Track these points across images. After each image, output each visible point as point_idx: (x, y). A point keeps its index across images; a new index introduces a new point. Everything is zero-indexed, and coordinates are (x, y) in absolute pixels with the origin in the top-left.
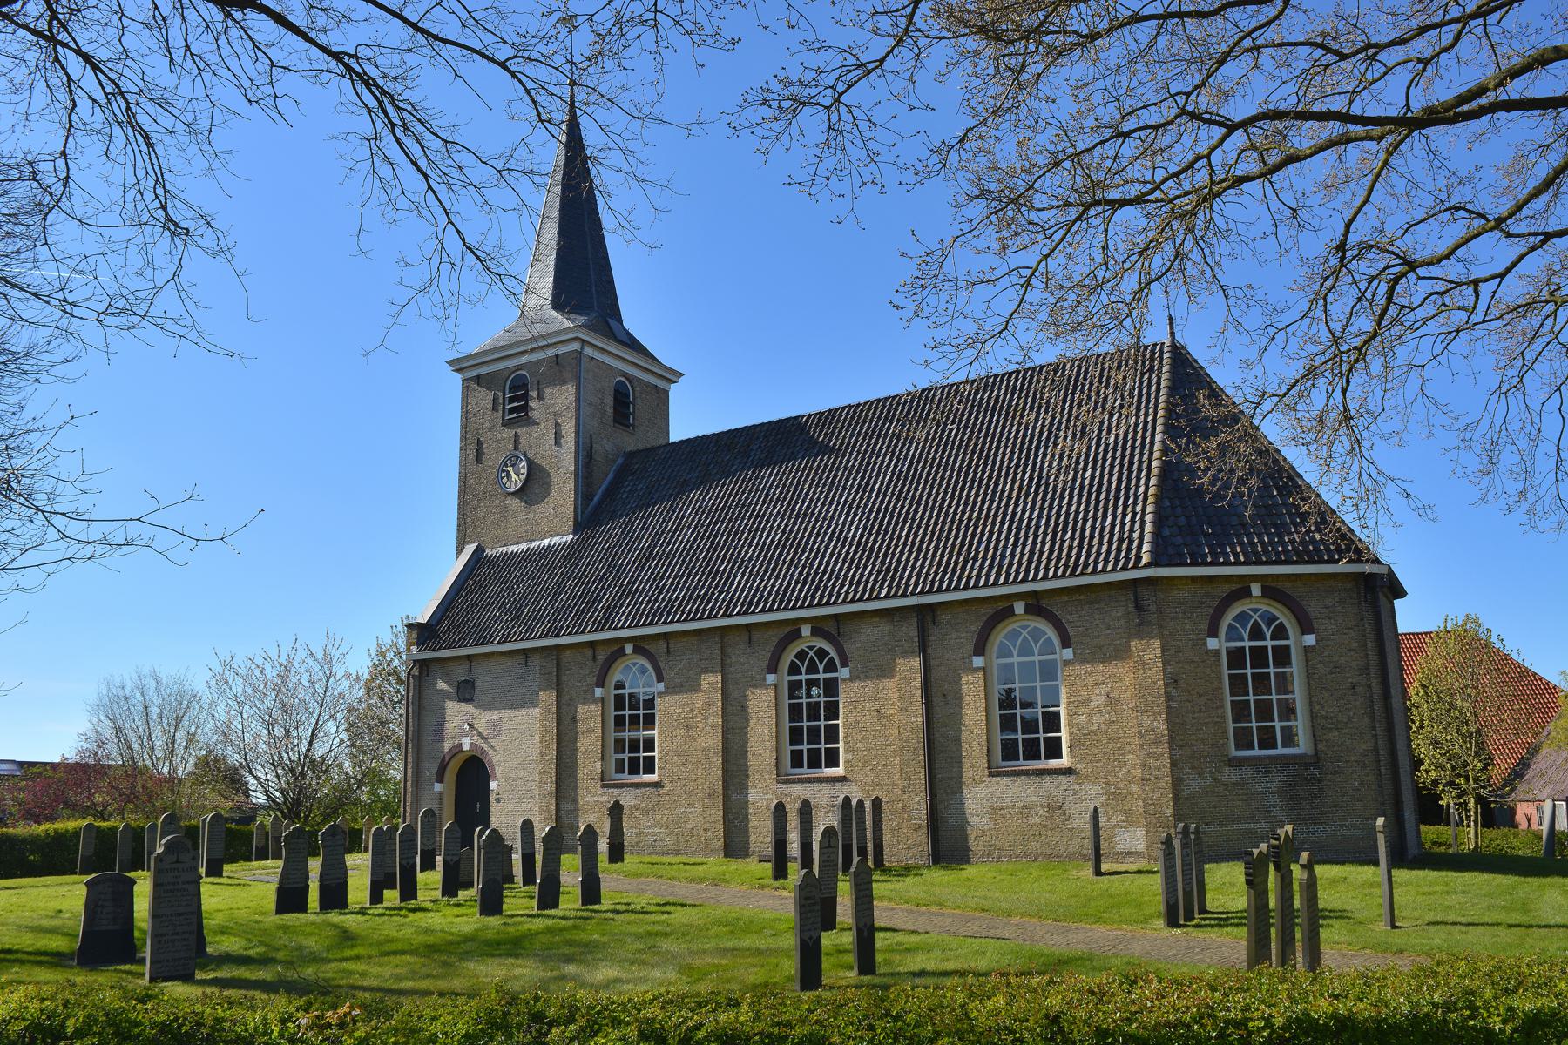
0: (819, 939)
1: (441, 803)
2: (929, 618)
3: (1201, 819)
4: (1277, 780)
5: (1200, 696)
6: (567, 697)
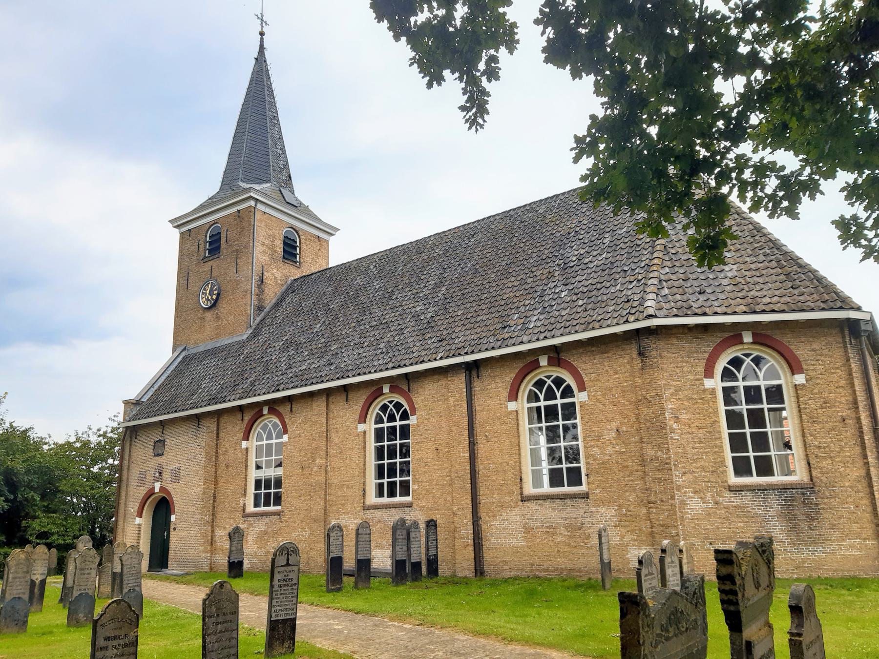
2: (474, 373)
3: (706, 538)
6: (224, 450)
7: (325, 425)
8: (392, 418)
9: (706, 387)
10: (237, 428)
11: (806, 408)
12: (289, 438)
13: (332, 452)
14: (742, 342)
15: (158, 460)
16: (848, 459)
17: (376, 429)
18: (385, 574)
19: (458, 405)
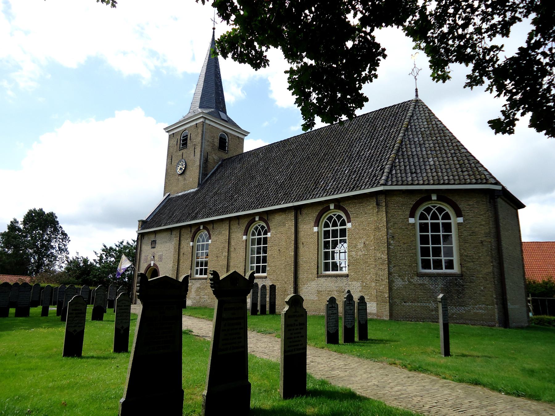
0: (49, 307)
2: (299, 212)
4: (440, 284)
5: (404, 244)
8: (259, 234)
9: (410, 222)
11: (462, 235)
12: (212, 242)
14: (431, 199)
15: (153, 250)
16: (482, 263)
19: (290, 228)
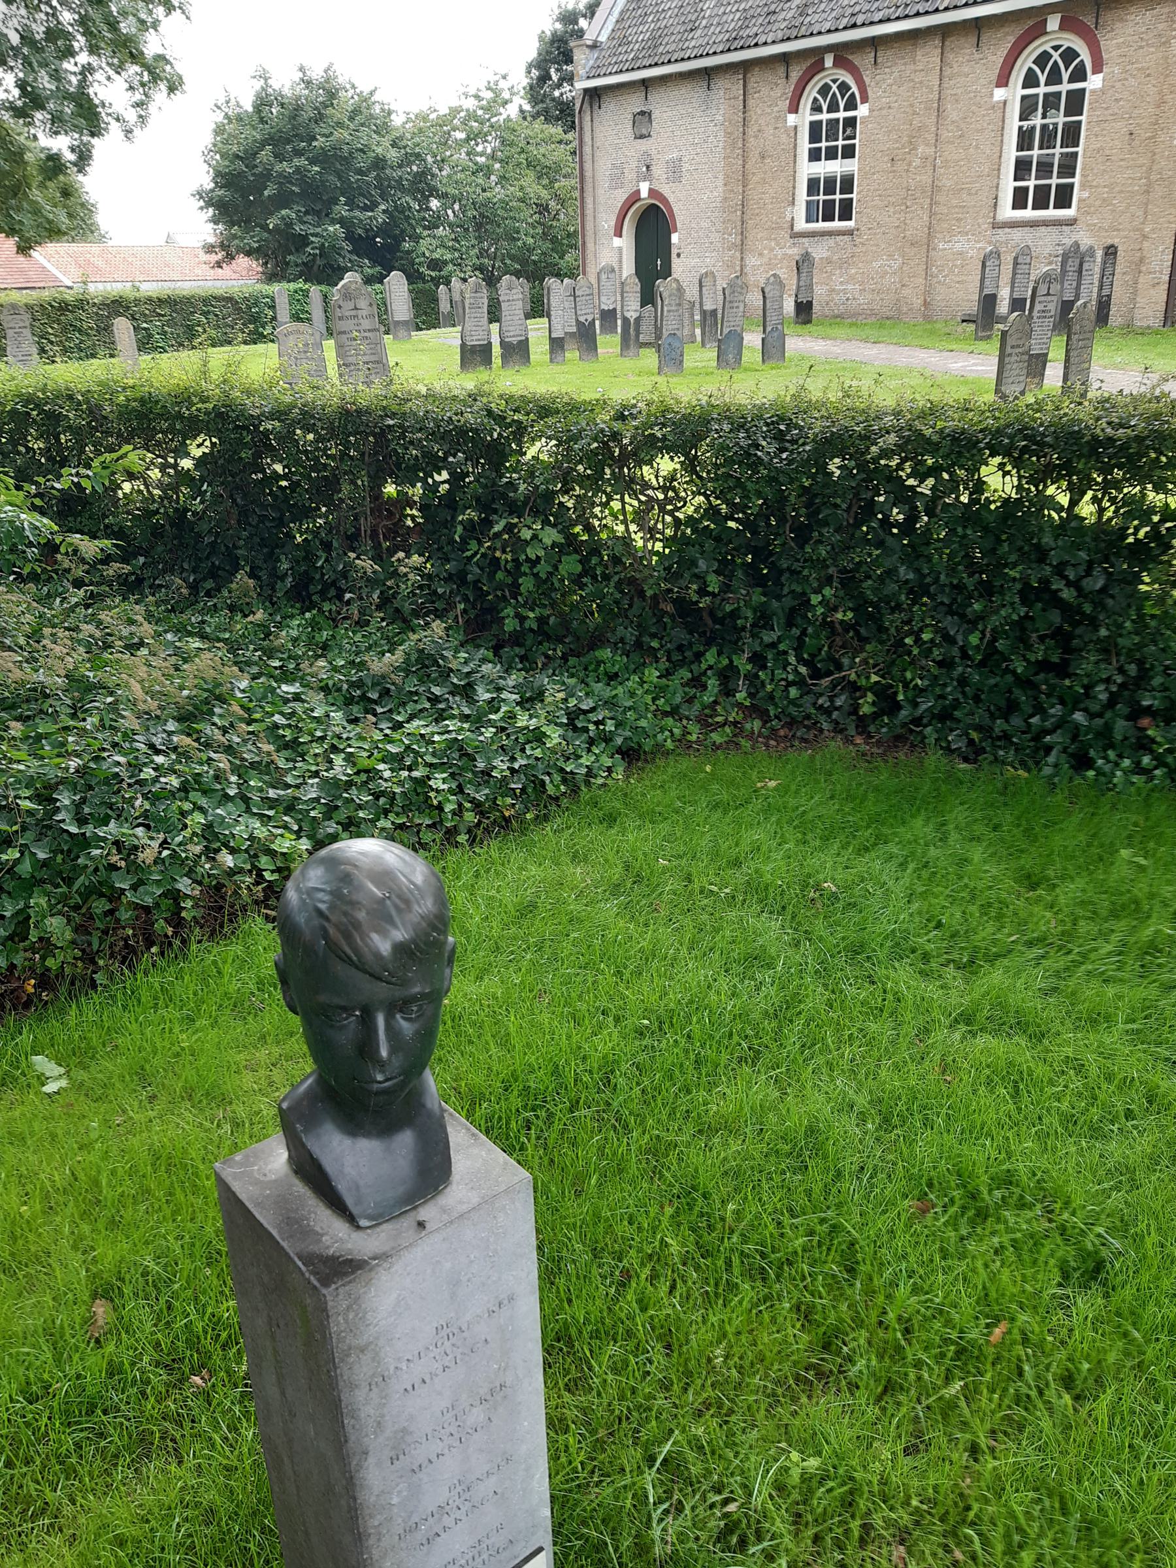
1: (620, 261)
6: (755, 128)
7: (936, 88)
10: (778, 92)
12: (871, 110)
13: (945, 135)
15: (643, 145)
17: (1024, 98)
18: (405, 323)
